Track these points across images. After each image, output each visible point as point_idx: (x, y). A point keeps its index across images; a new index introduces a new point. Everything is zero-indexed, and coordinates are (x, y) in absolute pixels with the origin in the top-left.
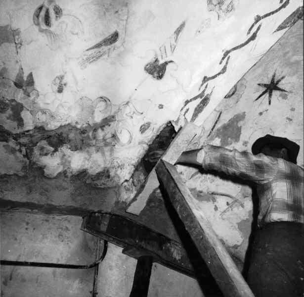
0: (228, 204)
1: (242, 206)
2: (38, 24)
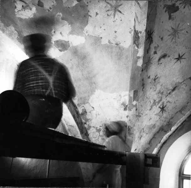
0: (23, 6)
1: (31, 9)
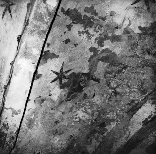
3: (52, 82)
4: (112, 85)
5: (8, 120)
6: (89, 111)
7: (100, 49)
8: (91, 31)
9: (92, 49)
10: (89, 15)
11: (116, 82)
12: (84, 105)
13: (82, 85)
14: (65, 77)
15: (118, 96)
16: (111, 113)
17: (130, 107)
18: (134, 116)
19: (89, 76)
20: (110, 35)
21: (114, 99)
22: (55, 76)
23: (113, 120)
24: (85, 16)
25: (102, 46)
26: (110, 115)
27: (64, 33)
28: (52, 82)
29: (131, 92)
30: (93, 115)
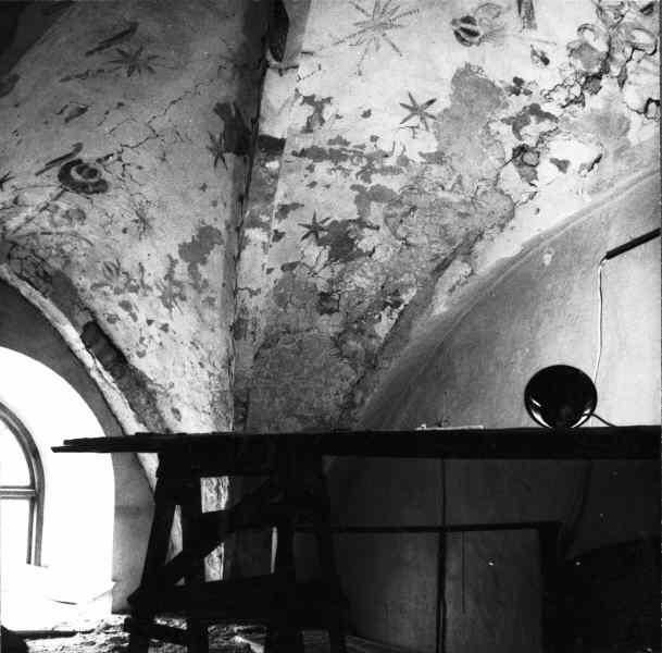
2: (471, 44)
3: (303, 238)
4: (327, 403)
5: (246, 302)
6: (370, 274)
7: (368, 186)
8: (346, 165)
9: (354, 187)
10: (337, 147)
11: (405, 229)
12: (361, 265)
13: (352, 237)
14: (322, 229)
15: (413, 250)
16: (406, 275)
17: (435, 265)
18: (440, 279)
19: (361, 223)
20: (377, 166)
21: (406, 253)
22: (307, 230)
23: (411, 285)
24: (331, 150)
25: (370, 182)
26: (405, 279)
27: (40, 565)
28: (303, 238)
29: (431, 242)
30: (377, 280)
